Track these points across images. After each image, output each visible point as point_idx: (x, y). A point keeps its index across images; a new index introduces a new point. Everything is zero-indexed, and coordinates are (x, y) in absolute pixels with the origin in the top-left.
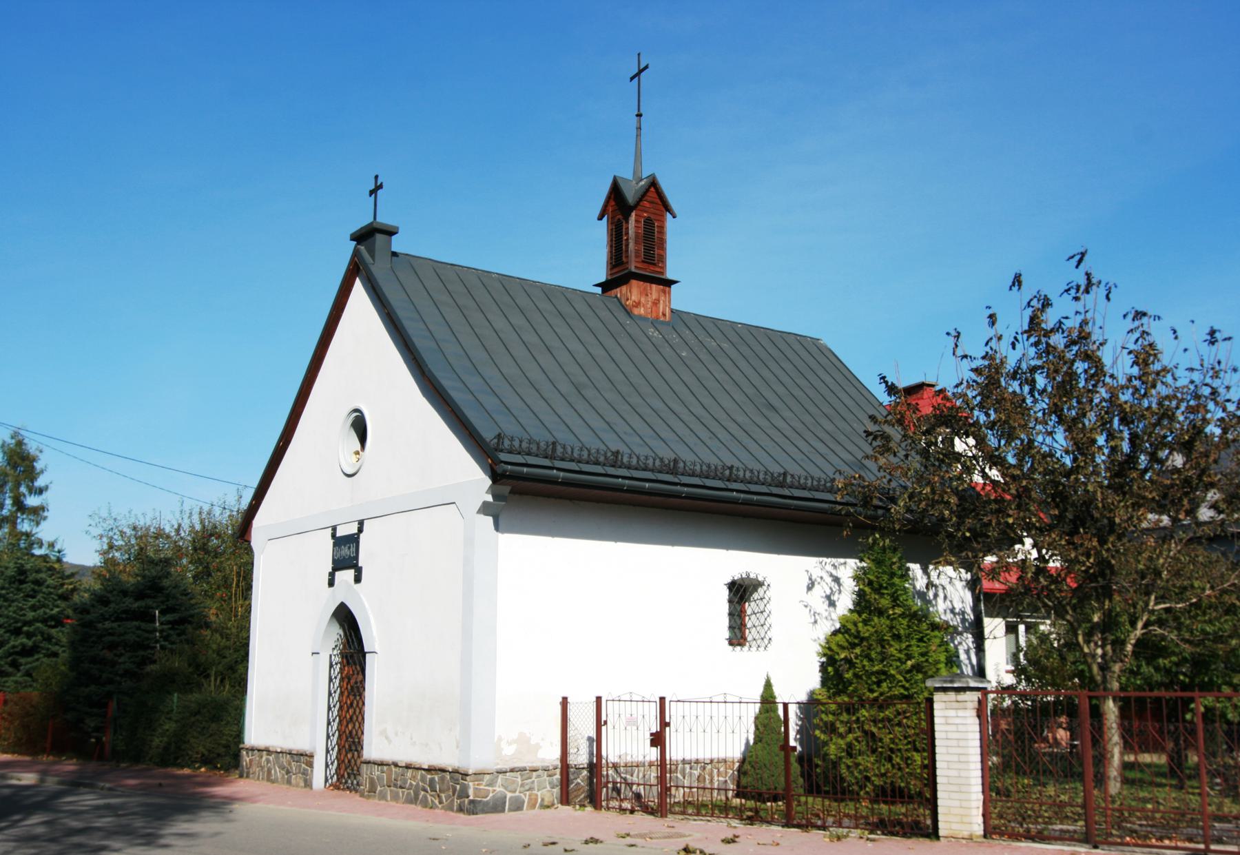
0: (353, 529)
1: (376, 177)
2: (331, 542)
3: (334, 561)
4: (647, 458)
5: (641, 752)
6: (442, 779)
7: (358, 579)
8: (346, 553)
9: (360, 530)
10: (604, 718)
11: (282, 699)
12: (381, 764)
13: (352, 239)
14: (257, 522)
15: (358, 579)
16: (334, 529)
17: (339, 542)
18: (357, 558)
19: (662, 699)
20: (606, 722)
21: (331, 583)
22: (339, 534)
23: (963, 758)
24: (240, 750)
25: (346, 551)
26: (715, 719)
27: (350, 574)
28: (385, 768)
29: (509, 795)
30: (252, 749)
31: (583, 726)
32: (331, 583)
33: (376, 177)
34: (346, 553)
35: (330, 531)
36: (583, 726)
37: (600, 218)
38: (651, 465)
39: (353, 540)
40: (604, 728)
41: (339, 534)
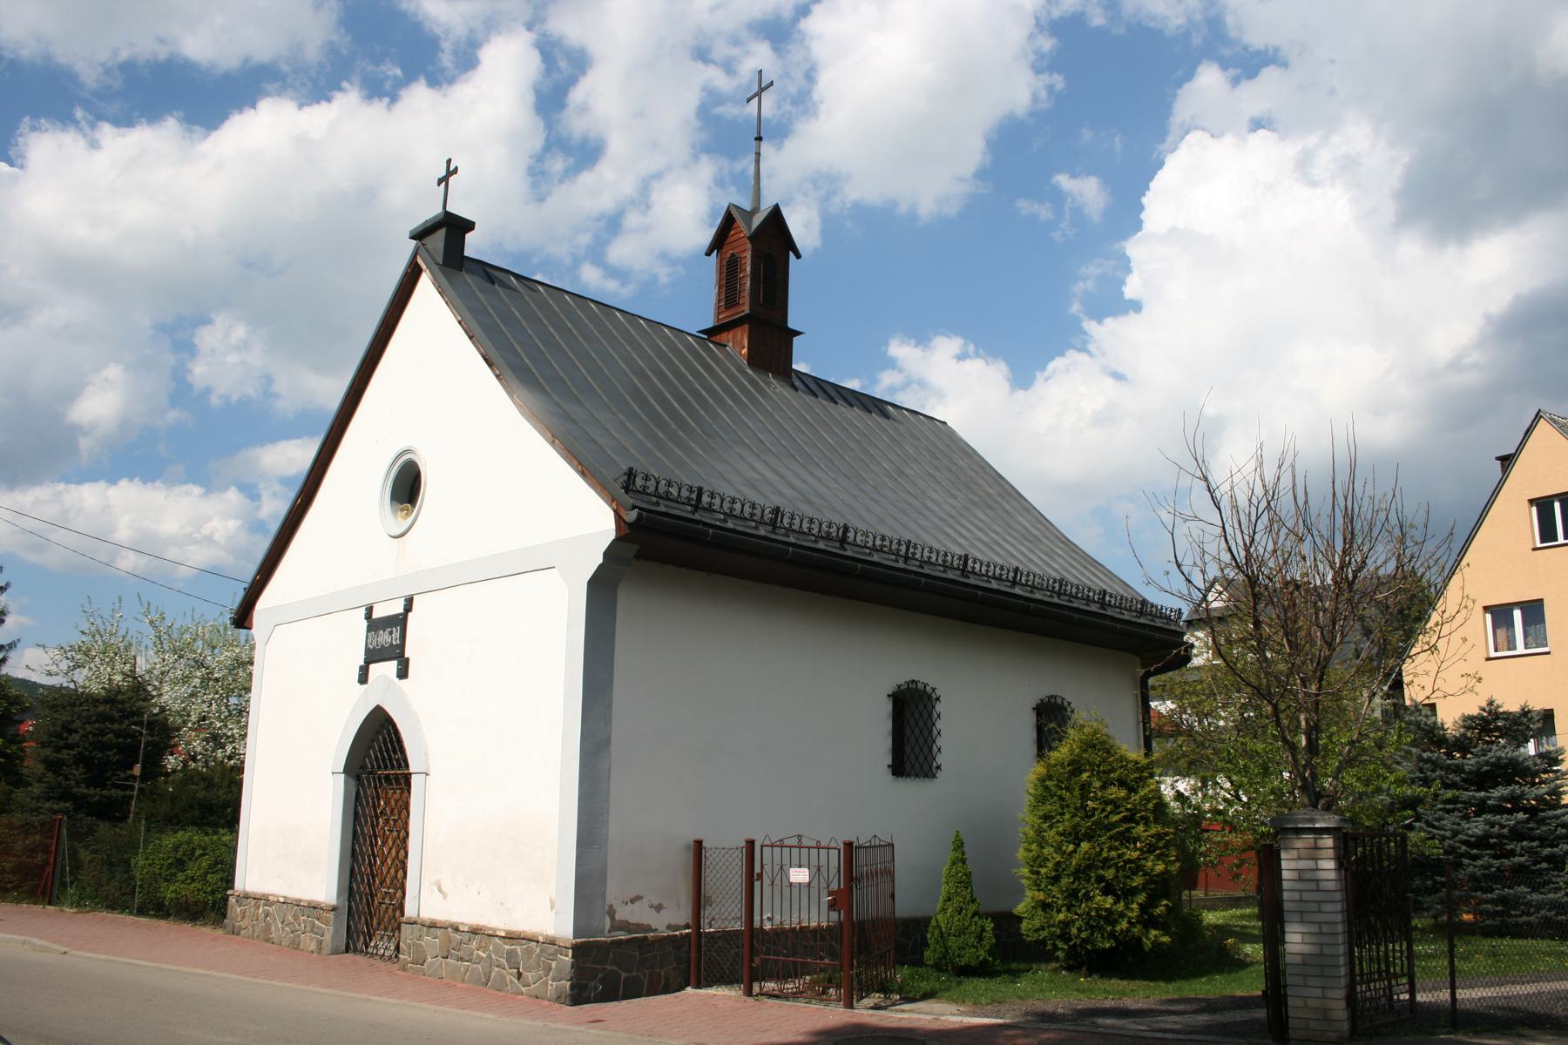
0: (399, 608)
1: (449, 162)
2: (365, 623)
3: (367, 651)
4: (733, 501)
5: (795, 919)
6: (529, 952)
7: (403, 673)
8: (387, 640)
9: (408, 607)
10: (757, 869)
11: (288, 839)
12: (433, 925)
13: (412, 238)
14: (261, 605)
15: (403, 673)
16: (370, 610)
17: (374, 625)
18: (402, 645)
19: (849, 845)
20: (760, 876)
21: (363, 679)
22: (375, 615)
23: (1325, 940)
24: (226, 899)
25: (386, 638)
26: (824, 870)
27: (392, 666)
28: (439, 932)
29: (624, 975)
30: (247, 896)
31: (725, 879)
32: (363, 679)
33: (449, 162)
34: (387, 640)
35: (363, 611)
36: (725, 879)
37: (708, 254)
38: (737, 512)
39: (400, 621)
40: (757, 884)
41: (375, 615)
